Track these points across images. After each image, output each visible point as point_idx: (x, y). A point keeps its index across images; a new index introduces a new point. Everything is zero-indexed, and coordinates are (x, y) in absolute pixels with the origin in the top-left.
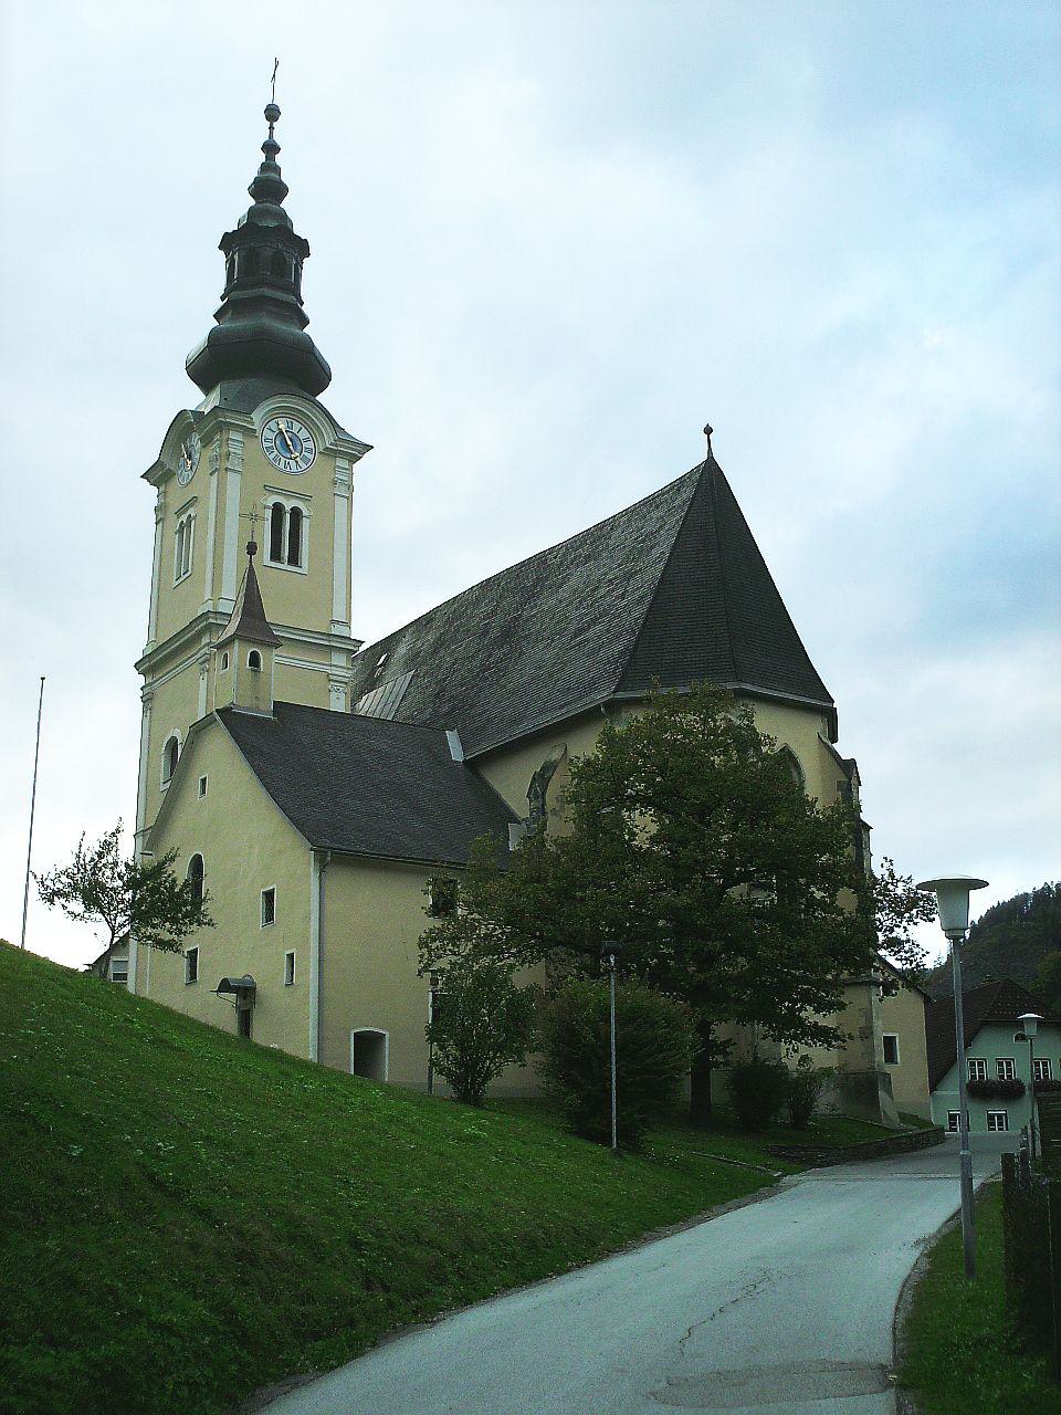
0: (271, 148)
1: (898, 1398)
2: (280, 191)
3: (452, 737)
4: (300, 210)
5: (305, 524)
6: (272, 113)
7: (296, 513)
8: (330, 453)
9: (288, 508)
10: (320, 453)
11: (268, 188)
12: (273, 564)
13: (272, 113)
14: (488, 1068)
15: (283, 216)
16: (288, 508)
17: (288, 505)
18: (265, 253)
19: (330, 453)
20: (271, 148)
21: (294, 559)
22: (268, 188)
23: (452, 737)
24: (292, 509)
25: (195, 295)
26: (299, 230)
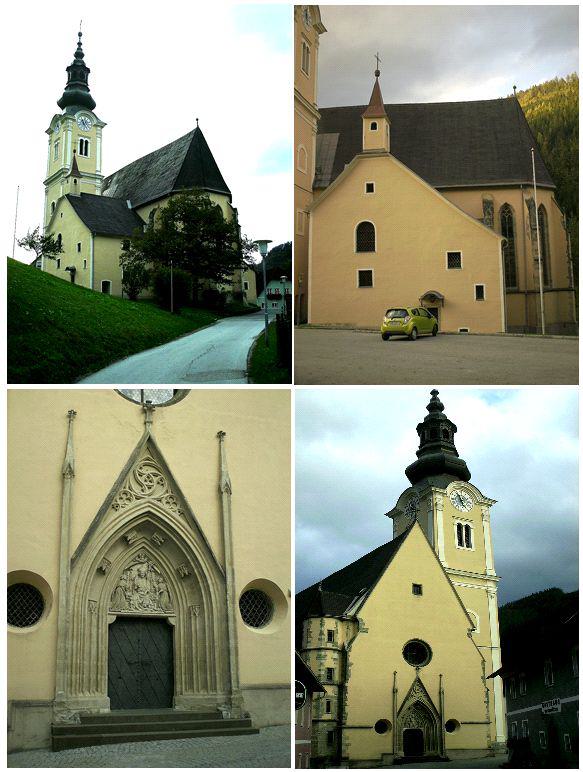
7: (467, 527)
17: (464, 524)
26: (415, 441)
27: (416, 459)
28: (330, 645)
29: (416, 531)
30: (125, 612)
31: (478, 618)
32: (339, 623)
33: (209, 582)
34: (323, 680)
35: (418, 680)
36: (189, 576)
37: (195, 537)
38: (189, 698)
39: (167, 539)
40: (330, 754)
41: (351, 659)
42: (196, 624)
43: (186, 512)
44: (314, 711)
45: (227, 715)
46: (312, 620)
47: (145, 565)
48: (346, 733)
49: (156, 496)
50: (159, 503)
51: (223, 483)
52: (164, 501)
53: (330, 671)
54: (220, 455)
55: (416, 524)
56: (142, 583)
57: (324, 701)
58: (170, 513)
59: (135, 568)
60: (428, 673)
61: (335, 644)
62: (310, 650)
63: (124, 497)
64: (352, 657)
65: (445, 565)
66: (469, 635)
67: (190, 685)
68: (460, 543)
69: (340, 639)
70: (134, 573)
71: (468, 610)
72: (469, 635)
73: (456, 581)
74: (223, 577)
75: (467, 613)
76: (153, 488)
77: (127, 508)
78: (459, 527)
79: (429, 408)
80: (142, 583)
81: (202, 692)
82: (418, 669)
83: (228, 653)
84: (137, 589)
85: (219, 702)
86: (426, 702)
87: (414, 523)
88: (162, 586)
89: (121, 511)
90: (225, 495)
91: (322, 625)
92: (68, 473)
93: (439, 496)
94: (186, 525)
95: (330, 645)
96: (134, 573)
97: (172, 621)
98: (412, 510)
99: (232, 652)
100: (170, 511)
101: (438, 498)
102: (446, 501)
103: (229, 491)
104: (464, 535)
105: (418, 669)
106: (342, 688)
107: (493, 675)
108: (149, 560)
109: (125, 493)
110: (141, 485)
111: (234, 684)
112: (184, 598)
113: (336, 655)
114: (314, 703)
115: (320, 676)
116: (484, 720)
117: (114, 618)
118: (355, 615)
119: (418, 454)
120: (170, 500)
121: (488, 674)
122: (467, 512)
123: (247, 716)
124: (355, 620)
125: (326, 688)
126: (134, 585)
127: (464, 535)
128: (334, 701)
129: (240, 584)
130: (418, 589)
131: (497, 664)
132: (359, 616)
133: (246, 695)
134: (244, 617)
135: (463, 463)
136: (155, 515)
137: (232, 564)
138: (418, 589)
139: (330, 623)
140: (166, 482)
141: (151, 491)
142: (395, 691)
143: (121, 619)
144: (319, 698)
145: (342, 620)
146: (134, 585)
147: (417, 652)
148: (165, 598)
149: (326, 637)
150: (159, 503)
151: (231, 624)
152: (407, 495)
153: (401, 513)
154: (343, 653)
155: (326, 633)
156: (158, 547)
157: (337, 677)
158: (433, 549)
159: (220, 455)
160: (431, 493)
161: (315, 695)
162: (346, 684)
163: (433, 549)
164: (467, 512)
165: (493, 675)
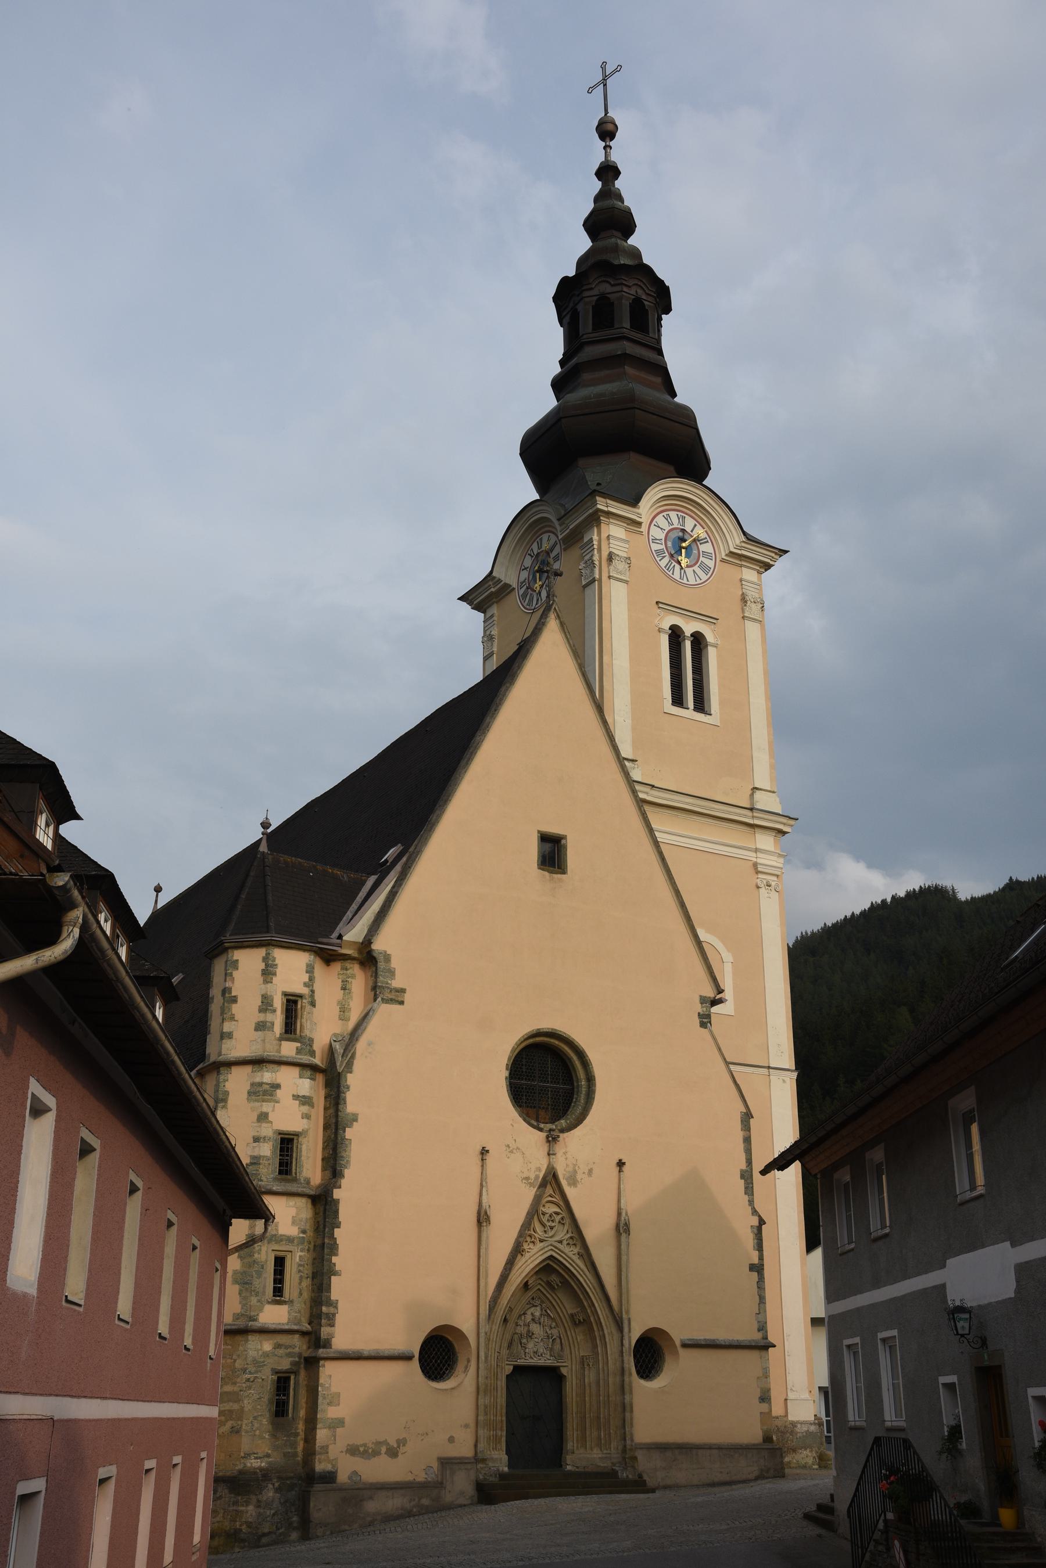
0: (608, 172)
1: (265, 1475)
2: (626, 224)
3: (180, 976)
4: (648, 242)
5: (712, 656)
6: (606, 131)
7: (698, 640)
8: (737, 558)
9: (688, 633)
10: (723, 561)
11: (609, 220)
12: (676, 710)
13: (606, 131)
14: (599, 1429)
15: (636, 254)
16: (688, 633)
17: (689, 628)
18: (611, 302)
19: (737, 558)
20: (608, 172)
21: (701, 705)
22: (609, 220)
23: (180, 976)
24: (692, 635)
25: (525, 365)
26: (552, 341)
27: (549, 402)
28: (289, 1049)
29: (552, 646)
30: (521, 1362)
31: (728, 968)
32: (319, 967)
33: (606, 1332)
34: (265, 1175)
35: (551, 1180)
36: (584, 1322)
37: (590, 1277)
38: (582, 1454)
39: (565, 1283)
40: (276, 1458)
41: (352, 1103)
42: (590, 1376)
43: (586, 1254)
44: (232, 1290)
45: (624, 1475)
46: (239, 955)
47: (538, 1308)
48: (334, 1376)
49: (557, 1238)
50: (559, 1245)
51: (623, 1221)
52: (565, 1242)
53: (287, 1143)
54: (619, 1188)
55: (552, 624)
56: (535, 1328)
57: (265, 1254)
58: (570, 1255)
59: (529, 1312)
60: (583, 1146)
61: (307, 1044)
62: (230, 1064)
63: (528, 1239)
64: (358, 1086)
65: (626, 751)
66: (705, 1020)
67: (583, 1440)
68: (678, 700)
69: (323, 1027)
70: (529, 1318)
71: (702, 935)
72: (705, 1020)
73: (657, 820)
74: (620, 1328)
75: (699, 943)
76: (555, 1229)
77: (533, 1252)
78: (676, 635)
79: (593, 225)
80: (535, 1328)
81: (595, 1451)
82: (552, 1139)
83: (625, 1408)
84: (530, 1335)
85: (615, 1461)
86: (578, 1267)
87: (544, 615)
88: (555, 1332)
89: (527, 1255)
90: (624, 1236)
91: (268, 972)
92: (482, 1219)
93: (614, 530)
94: (585, 1270)
95: (289, 1049)
96: (529, 1318)
97: (564, 1371)
98: (536, 580)
99: (628, 1408)
100: (570, 1254)
101: (612, 537)
102: (634, 537)
103: (627, 1231)
104: (688, 667)
105: (552, 1139)
106: (323, 1205)
107: (781, 1163)
108: (542, 1302)
109: (530, 1236)
110: (544, 1225)
111: (628, 1442)
112: (578, 1345)
113: (305, 1085)
114: (234, 1263)
115: (256, 1161)
116: (751, 1335)
117: (511, 1368)
118: (367, 942)
119: (559, 385)
120: (571, 1242)
121: (758, 1165)
122: (702, 587)
123: (640, 1476)
124: (368, 958)
125: (273, 1204)
126: (529, 1331)
127: (688, 667)
128: (297, 1259)
129: (636, 1333)
130: (552, 853)
131: (783, 1128)
132: (379, 945)
133: (640, 1455)
134: (638, 1373)
135: (686, 419)
136: (578, 1280)
137: (628, 1312)
138: (552, 853)
139: (293, 967)
140: (567, 1221)
141: (553, 1232)
142: (482, 1219)
143: (518, 1369)
144: (252, 1241)
145: (329, 958)
146: (529, 1331)
147: (548, 1079)
148: (557, 1347)
149: (278, 1020)
150: (559, 1245)
151: (626, 1379)
152: (525, 526)
153: (505, 590)
154: (331, 1075)
155: (278, 1003)
156: (553, 1288)
157: (310, 1166)
158: (599, 708)
159: (619, 1188)
160: (595, 519)
161: (240, 1229)
162: (337, 1194)
163: (599, 708)
164: (702, 587)
165: (781, 1163)
